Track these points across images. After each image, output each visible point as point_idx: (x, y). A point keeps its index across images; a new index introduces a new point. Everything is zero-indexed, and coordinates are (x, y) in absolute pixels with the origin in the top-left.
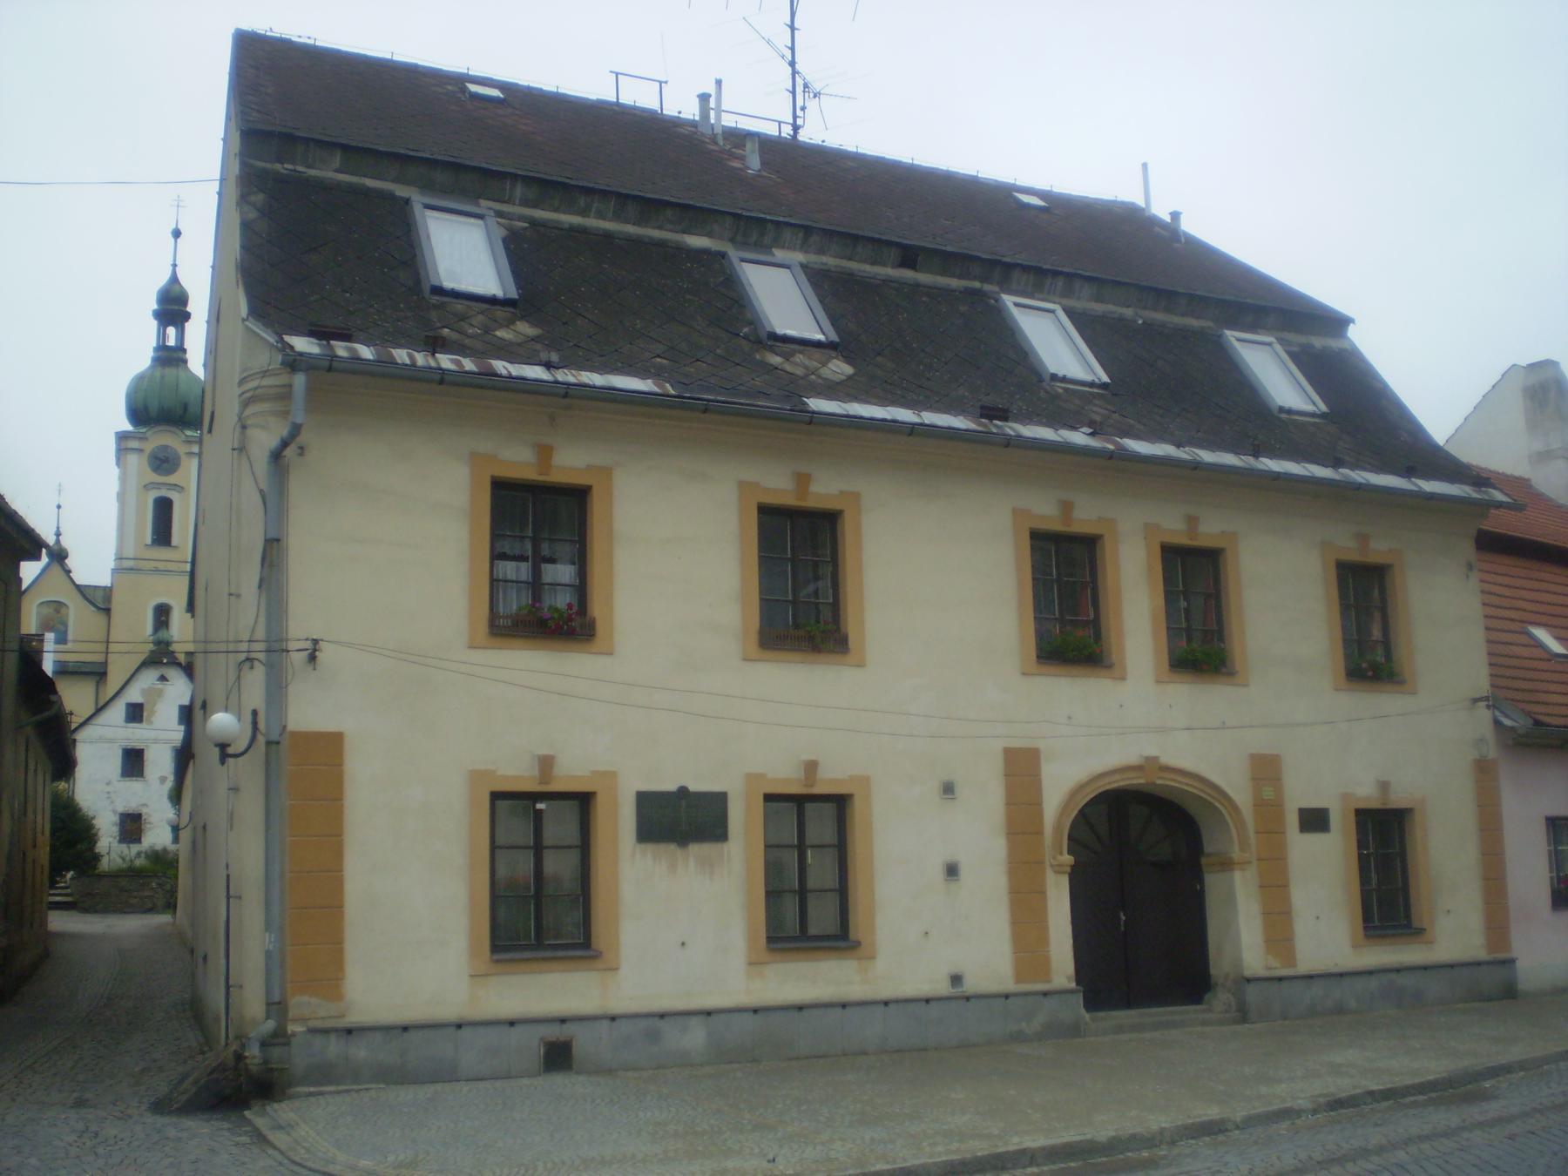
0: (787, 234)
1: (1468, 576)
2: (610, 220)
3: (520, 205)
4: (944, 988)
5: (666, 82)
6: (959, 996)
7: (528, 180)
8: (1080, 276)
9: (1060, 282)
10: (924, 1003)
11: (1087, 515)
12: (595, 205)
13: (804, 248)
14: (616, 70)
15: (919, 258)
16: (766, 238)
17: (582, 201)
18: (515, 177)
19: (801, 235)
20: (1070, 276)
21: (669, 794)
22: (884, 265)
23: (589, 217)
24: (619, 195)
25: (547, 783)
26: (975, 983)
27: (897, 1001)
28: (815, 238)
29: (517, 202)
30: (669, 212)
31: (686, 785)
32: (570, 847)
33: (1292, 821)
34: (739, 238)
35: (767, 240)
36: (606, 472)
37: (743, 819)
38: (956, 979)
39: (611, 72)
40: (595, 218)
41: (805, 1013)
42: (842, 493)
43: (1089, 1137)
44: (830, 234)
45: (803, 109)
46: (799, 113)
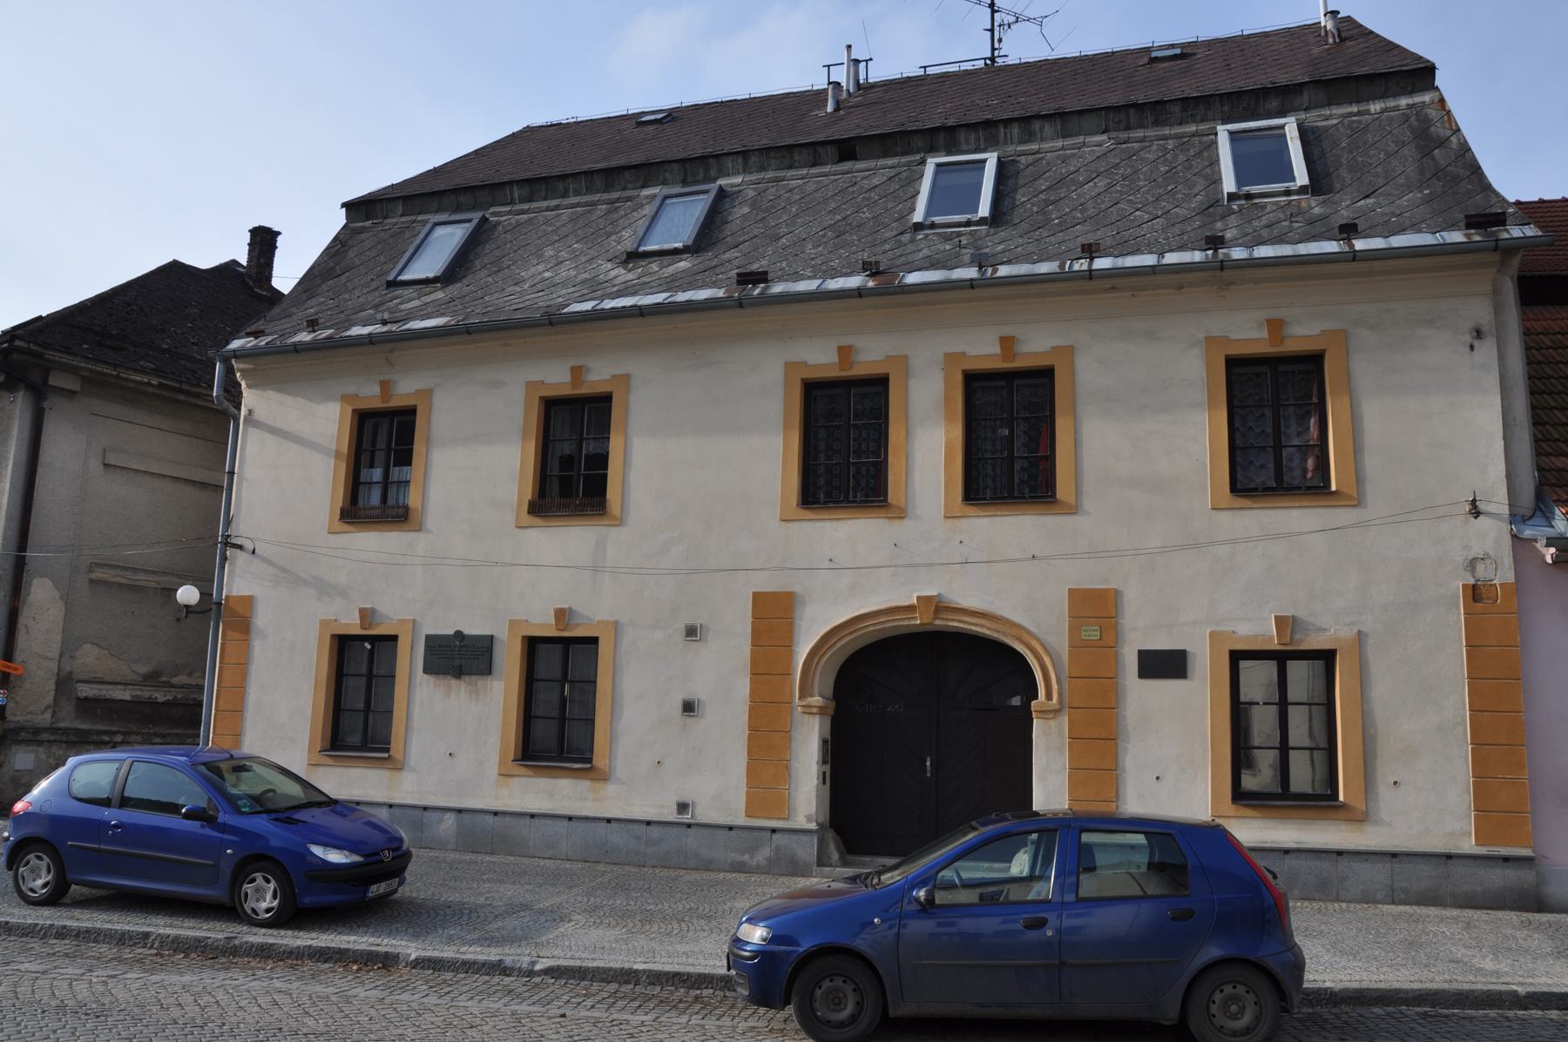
0: (729, 163)
1: (1472, 347)
2: (585, 195)
3: (520, 203)
4: (671, 815)
5: (871, 59)
6: (684, 822)
7: (521, 182)
8: (1038, 117)
9: (1015, 130)
10: (727, 829)
11: (872, 353)
12: (571, 187)
13: (746, 170)
14: (826, 64)
15: (857, 148)
16: (712, 171)
17: (561, 186)
18: (510, 183)
19: (740, 160)
20: (1025, 121)
21: (448, 637)
22: (825, 164)
23: (569, 197)
24: (585, 173)
25: (1291, 643)
26: (706, 812)
27: (618, 820)
28: (753, 159)
29: (517, 202)
30: (627, 174)
31: (462, 630)
32: (541, 680)
33: (1131, 663)
34: (689, 179)
35: (713, 173)
36: (427, 394)
37: (509, 660)
38: (682, 807)
39: (824, 66)
40: (575, 196)
41: (536, 821)
42: (614, 377)
43: (548, 965)
44: (766, 151)
45: (1000, 40)
46: (996, 45)
